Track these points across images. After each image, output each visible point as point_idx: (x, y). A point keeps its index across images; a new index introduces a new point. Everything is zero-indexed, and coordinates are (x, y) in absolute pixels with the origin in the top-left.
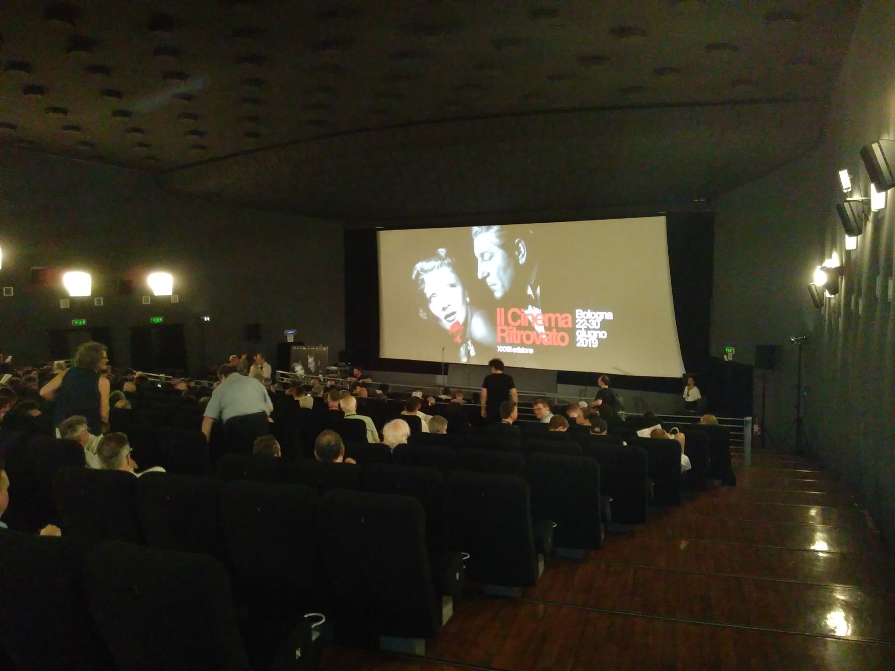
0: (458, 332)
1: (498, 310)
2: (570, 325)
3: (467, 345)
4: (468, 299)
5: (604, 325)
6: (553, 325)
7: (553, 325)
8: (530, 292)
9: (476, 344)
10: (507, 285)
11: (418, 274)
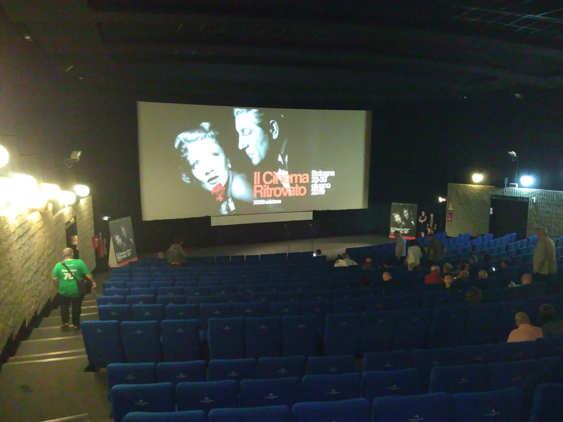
0: (220, 192)
1: (255, 173)
2: (307, 181)
3: (228, 202)
5: (330, 179)
6: (296, 182)
7: (296, 182)
11: (181, 143)
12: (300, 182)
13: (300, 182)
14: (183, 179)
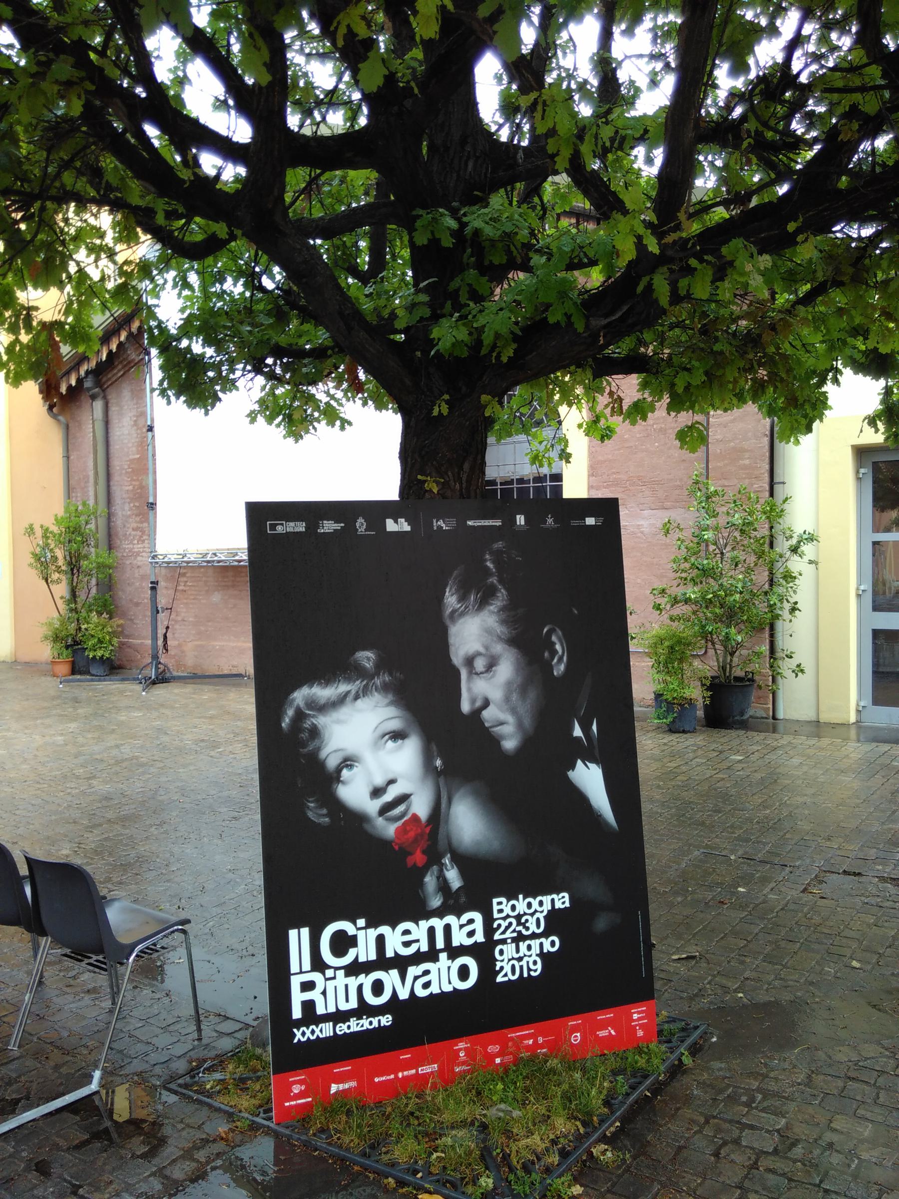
0: (416, 840)
1: (293, 934)
2: (480, 937)
3: (442, 866)
4: (438, 763)
5: (555, 922)
6: (440, 944)
7: (440, 944)
8: (578, 732)
9: (463, 861)
10: (527, 722)
11: (300, 716)
12: (455, 943)
13: (455, 943)
14: (310, 814)
